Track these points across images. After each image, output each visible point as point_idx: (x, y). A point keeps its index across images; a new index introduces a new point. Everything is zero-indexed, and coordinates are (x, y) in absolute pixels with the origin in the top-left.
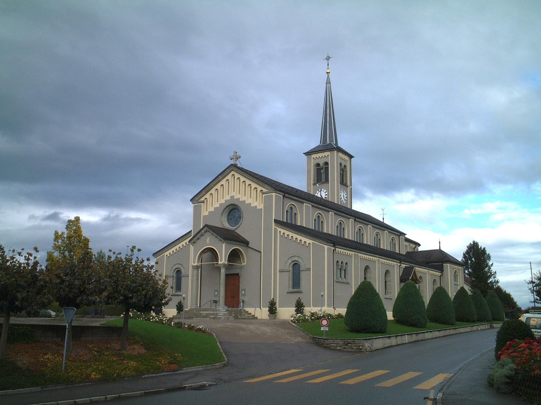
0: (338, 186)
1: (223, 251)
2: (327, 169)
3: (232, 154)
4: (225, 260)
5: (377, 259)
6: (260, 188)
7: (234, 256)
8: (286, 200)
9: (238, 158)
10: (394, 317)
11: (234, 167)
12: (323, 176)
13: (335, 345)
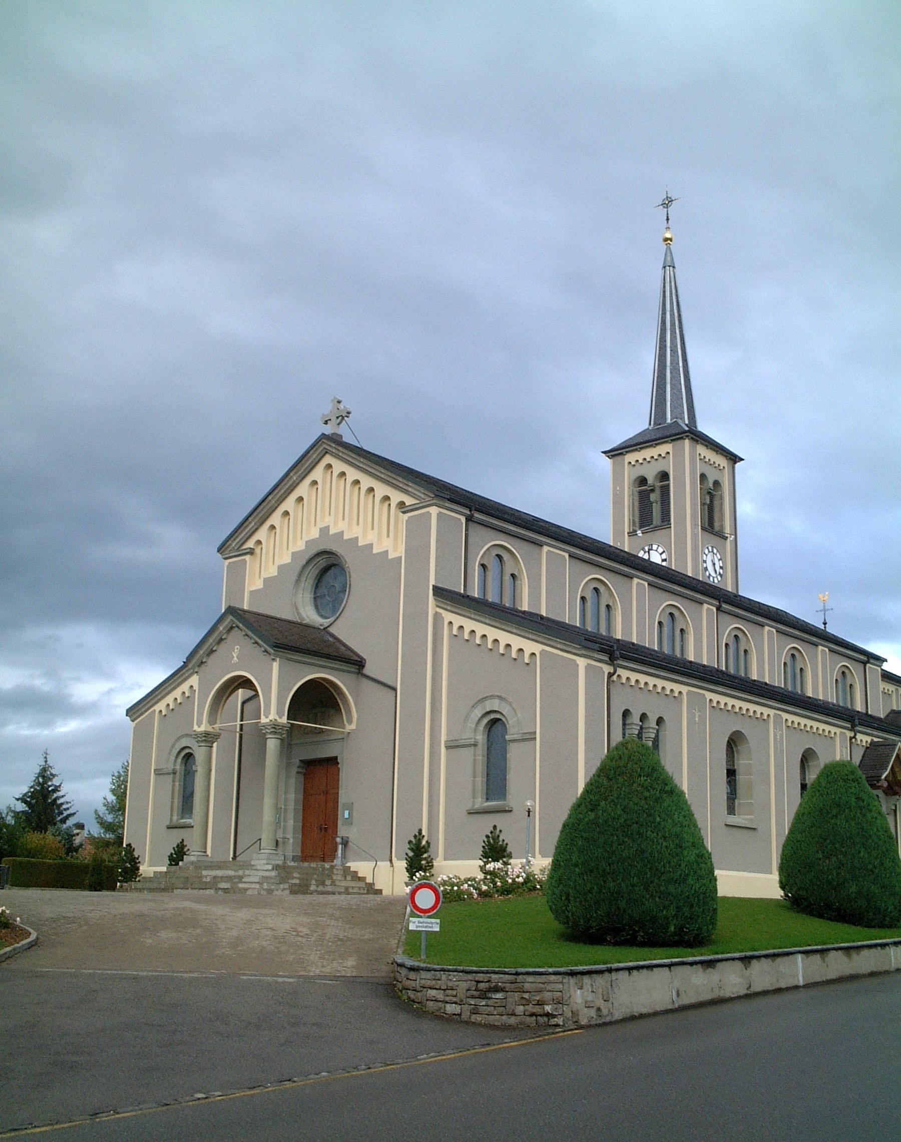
0: (694, 536)
1: (276, 685)
2: (665, 491)
3: (327, 409)
4: (280, 713)
5: (772, 712)
6: (397, 497)
7: (316, 703)
8: (478, 532)
9: (342, 418)
10: (783, 887)
11: (331, 444)
12: (656, 510)
13: (440, 995)
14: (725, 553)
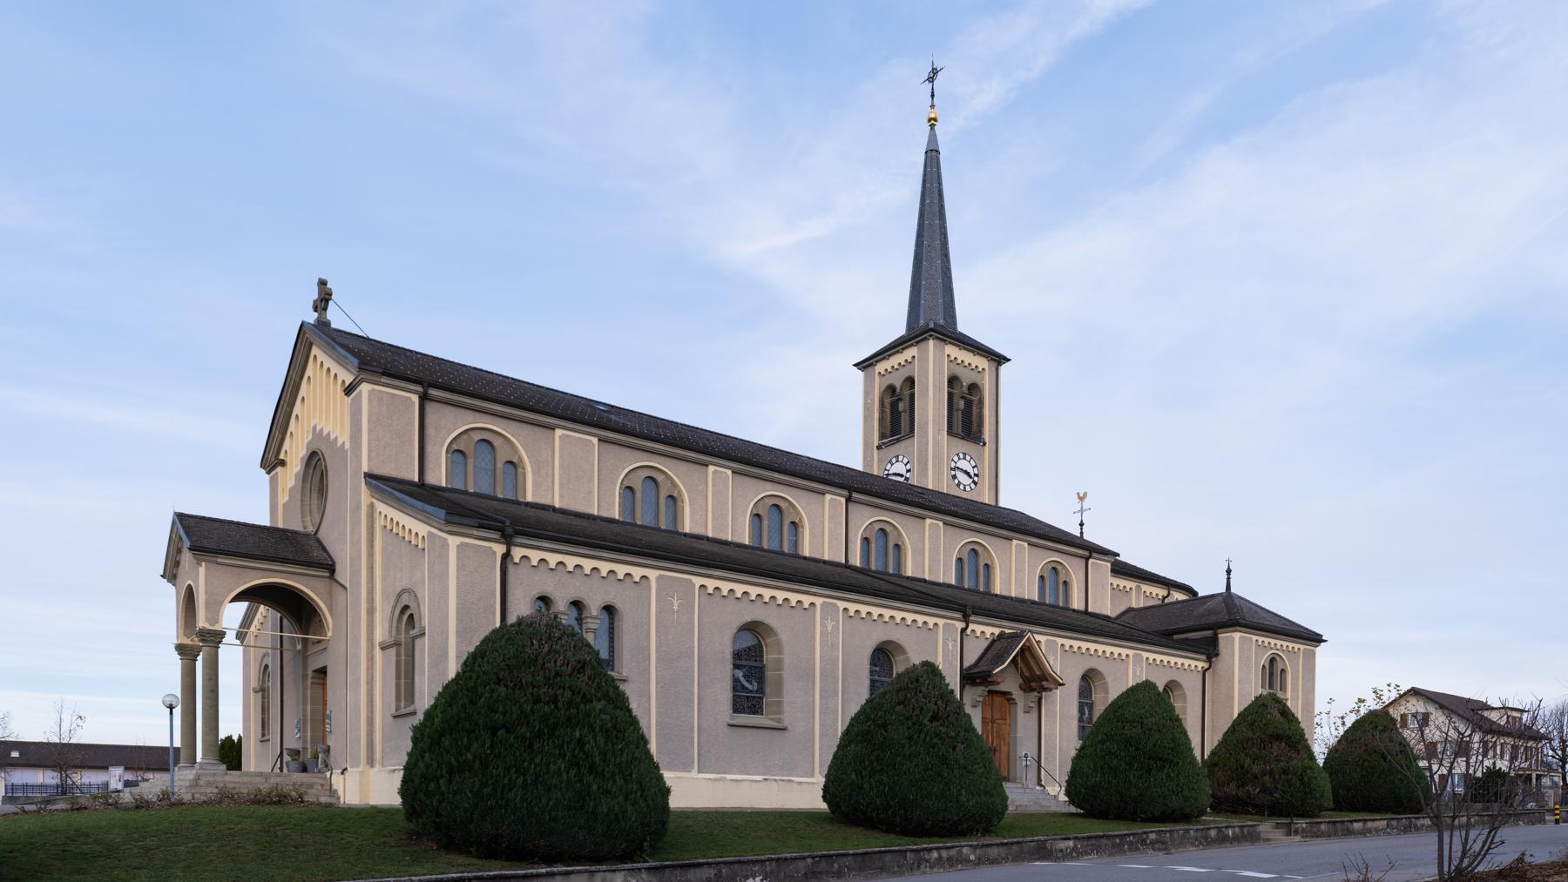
0: (937, 444)
12: (904, 418)
14: (982, 460)
